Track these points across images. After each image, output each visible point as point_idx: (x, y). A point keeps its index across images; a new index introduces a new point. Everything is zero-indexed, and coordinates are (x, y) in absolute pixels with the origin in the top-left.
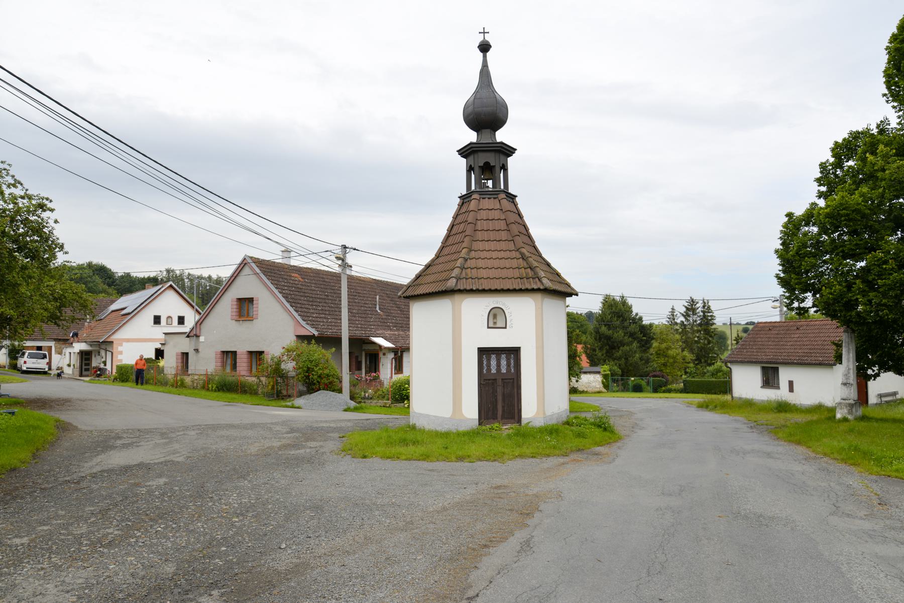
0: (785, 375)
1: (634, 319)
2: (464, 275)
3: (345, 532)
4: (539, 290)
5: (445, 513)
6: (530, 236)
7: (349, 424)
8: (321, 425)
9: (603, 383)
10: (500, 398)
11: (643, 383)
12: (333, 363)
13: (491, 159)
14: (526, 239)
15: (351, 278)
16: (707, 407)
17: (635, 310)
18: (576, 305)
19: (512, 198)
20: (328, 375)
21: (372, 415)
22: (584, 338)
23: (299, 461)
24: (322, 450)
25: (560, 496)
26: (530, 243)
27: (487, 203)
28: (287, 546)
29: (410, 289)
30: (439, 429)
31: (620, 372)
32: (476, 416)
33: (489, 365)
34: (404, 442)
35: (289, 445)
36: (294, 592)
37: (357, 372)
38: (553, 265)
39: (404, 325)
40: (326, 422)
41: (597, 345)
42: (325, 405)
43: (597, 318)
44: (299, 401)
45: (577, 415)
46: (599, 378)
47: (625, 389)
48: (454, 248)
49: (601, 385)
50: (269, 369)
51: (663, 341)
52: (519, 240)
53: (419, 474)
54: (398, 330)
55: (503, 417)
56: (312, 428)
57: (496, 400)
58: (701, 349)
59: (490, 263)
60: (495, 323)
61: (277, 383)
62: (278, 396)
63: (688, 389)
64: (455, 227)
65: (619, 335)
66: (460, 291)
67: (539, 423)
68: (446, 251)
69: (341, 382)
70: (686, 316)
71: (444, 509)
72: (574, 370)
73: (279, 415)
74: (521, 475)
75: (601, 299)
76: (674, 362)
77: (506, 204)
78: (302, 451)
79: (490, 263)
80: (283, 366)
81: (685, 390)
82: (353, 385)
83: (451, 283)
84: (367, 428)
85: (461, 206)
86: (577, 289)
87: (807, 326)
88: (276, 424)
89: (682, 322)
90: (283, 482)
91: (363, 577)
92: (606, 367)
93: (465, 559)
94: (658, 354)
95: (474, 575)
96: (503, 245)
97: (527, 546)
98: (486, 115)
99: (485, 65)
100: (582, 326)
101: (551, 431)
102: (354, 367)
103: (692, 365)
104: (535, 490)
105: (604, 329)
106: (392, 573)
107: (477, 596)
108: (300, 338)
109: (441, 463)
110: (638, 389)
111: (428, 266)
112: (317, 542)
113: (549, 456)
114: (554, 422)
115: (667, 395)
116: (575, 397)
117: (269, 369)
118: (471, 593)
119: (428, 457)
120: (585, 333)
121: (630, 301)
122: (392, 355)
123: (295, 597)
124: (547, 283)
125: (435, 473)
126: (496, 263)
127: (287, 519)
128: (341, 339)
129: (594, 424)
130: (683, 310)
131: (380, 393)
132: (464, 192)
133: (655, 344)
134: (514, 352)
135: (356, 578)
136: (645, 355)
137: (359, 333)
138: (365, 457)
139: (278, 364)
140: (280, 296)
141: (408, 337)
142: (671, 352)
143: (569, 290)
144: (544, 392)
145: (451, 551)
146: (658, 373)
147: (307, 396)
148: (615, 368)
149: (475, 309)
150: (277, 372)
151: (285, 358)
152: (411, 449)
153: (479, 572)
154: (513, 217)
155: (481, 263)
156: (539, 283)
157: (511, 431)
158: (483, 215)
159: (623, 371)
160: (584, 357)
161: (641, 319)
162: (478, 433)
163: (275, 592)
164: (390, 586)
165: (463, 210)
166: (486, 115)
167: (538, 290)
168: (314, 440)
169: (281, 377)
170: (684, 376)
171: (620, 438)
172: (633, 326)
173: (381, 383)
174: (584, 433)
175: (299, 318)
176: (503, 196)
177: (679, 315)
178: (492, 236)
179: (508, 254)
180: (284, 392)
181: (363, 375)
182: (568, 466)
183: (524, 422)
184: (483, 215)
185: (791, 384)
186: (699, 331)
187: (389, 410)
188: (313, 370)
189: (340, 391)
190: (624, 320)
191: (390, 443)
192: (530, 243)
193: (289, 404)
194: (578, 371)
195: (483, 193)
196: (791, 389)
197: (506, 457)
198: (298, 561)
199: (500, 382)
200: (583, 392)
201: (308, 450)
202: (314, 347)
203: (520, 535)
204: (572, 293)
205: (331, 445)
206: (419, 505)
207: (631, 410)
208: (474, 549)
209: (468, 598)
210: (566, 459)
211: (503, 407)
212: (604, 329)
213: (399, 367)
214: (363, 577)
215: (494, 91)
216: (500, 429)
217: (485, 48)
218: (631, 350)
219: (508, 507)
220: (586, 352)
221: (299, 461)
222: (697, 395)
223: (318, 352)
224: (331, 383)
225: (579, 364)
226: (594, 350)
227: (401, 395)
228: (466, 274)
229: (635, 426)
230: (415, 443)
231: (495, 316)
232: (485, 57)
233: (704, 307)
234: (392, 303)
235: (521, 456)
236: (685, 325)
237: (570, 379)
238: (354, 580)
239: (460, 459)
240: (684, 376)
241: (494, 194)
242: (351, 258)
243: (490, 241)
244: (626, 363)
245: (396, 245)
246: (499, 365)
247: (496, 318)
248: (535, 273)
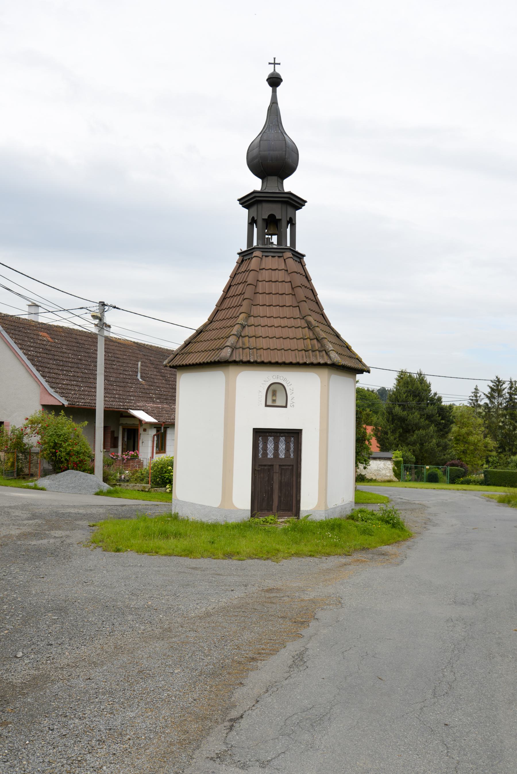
1: (432, 399)
2: (240, 344)
3: (92, 639)
4: (325, 365)
5: (208, 619)
6: (318, 303)
7: (101, 510)
8: (69, 510)
9: (394, 471)
10: (276, 486)
11: (439, 472)
12: (85, 439)
13: (277, 211)
14: (314, 307)
15: (108, 340)
16: (509, 502)
17: (434, 389)
18: (364, 381)
19: (299, 257)
20: (78, 452)
21: (128, 501)
22: (374, 419)
23: (41, 553)
24: (68, 541)
25: (339, 602)
26: (318, 310)
27: (270, 262)
28: (24, 654)
29: (178, 357)
30: (204, 520)
31: (414, 459)
32: (249, 507)
33: (265, 449)
34: (165, 534)
35: (30, 534)
36: (30, 710)
37: (112, 450)
38: (343, 336)
39: (170, 397)
40: (74, 507)
41: (390, 427)
42: (74, 488)
43: (391, 396)
44: (44, 482)
45: (363, 507)
46: (389, 465)
47: (419, 478)
48: (230, 313)
49: (392, 474)
50: (9, 442)
51: (464, 425)
52: (306, 307)
53: (180, 572)
54: (161, 402)
55: (279, 509)
56: (57, 514)
57: (272, 489)
58: (506, 436)
59: (271, 332)
60: (274, 401)
61: (18, 460)
62: (18, 475)
63: (489, 480)
64: (232, 288)
65: (415, 416)
66: (235, 363)
67: (320, 516)
69: (93, 460)
70: (491, 397)
71: (208, 615)
72: (362, 455)
73: (19, 498)
74: (296, 576)
75: (396, 375)
76: (475, 449)
77: (292, 264)
78: (45, 541)
79: (271, 332)
80: (25, 440)
81: (486, 482)
82: (107, 464)
83: (226, 354)
84: (121, 515)
85: (240, 263)
86: (367, 361)
88: (16, 508)
89: (486, 404)
90: (21, 578)
91: (111, 693)
92: (398, 453)
93: (229, 673)
94: (457, 440)
95: (238, 693)
96: (287, 312)
97: (300, 660)
98: (273, 160)
99: (274, 101)
100: (373, 404)
101: (333, 526)
102: (109, 444)
103: (494, 453)
104: (312, 595)
105: (397, 409)
106: (146, 689)
107: (241, 717)
108: (47, 408)
109: (207, 561)
110: (433, 479)
111: (200, 332)
112: (59, 651)
113: (329, 555)
114: (336, 516)
115: (465, 487)
116: (362, 486)
117: (9, 442)
118: (234, 714)
119: (191, 552)
120: (376, 413)
121: (428, 379)
122: (153, 432)
123: (32, 716)
124: (335, 358)
125: (199, 572)
126: (278, 332)
127: (25, 622)
128: (95, 410)
129: (382, 519)
130: (487, 390)
131: (138, 474)
132: (245, 248)
133: (455, 428)
134: (295, 435)
135: (104, 694)
136: (443, 441)
137: (116, 405)
138: (118, 550)
139: (20, 438)
140: (24, 358)
141: (173, 411)
142: (472, 438)
143: (360, 366)
144: (326, 483)
145: (214, 664)
146: (457, 462)
147: (53, 476)
148: (409, 454)
149: (252, 383)
150: (18, 446)
151: (28, 431)
152: (172, 541)
153: (245, 689)
154: (299, 280)
155: (260, 331)
156: (326, 357)
157: (287, 525)
158: (265, 275)
159: (417, 459)
160: (374, 441)
161: (440, 399)
162: (250, 526)
163: (9, 709)
164: (142, 704)
165: (243, 269)
166: (273, 160)
167: (325, 365)
168: (59, 528)
169: (23, 453)
170: (485, 466)
171: (410, 536)
172: (430, 407)
173: (140, 464)
174: (369, 529)
175: (46, 385)
176: (289, 254)
177: (483, 396)
178: (275, 299)
179: (292, 322)
180: (26, 471)
181: (120, 453)
182: (351, 567)
183: (302, 515)
184: (265, 275)
186: (504, 415)
187: (148, 495)
188: (61, 446)
189: (92, 471)
190: (421, 400)
191: (148, 535)
192: (318, 310)
193: (31, 484)
194: (366, 456)
195: (267, 250)
197: (281, 555)
198: (36, 672)
199: (277, 468)
200: (371, 480)
201: (52, 541)
202: (62, 419)
203: (293, 647)
204: (363, 370)
205: (79, 535)
206: (179, 609)
207: (424, 503)
208: (239, 663)
209: (231, 720)
210: (348, 559)
211: (280, 497)
212: (397, 409)
213: (161, 446)
214: (111, 693)
215: (283, 133)
216: (276, 523)
217: (274, 81)
218: (427, 435)
219: (280, 614)
220: (376, 435)
221: (41, 553)
222: (498, 488)
223: (68, 425)
224: (81, 461)
225: (367, 448)
226: (386, 433)
227: (163, 478)
228: (243, 343)
229: (428, 522)
230: (177, 535)
231: (274, 393)
232: (274, 92)
233: (511, 388)
234: (158, 371)
235: (297, 554)
236: (489, 408)
237: (357, 466)
238: (101, 697)
239: (229, 556)
240: (485, 466)
241: (279, 251)
242: (109, 317)
243: (270, 307)
244: (421, 449)
245: (165, 303)
246: (276, 448)
247: (275, 395)
248: (323, 346)
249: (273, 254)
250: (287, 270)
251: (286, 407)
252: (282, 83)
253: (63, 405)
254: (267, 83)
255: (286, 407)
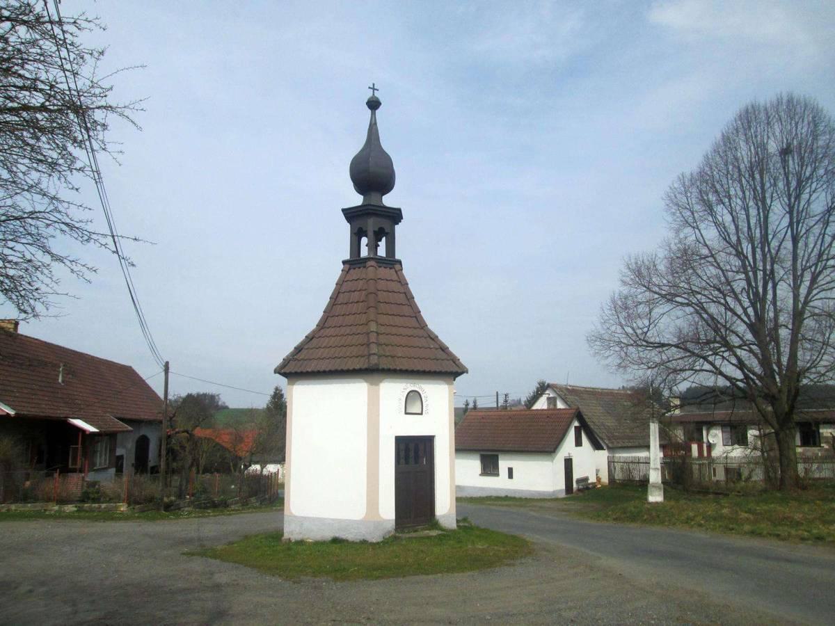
0: (504, 464)
32: (393, 517)
68: (330, 322)
86: (464, 360)
87: (494, 437)
98: (372, 175)
143: (455, 369)
166: (372, 175)
185: (510, 471)
196: (511, 475)
217: (374, 104)
232: (373, 114)
249: (384, 265)
250: (400, 282)
251: (421, 414)
252: (381, 107)
253: (824, 525)
254: (366, 106)
255: (421, 414)
